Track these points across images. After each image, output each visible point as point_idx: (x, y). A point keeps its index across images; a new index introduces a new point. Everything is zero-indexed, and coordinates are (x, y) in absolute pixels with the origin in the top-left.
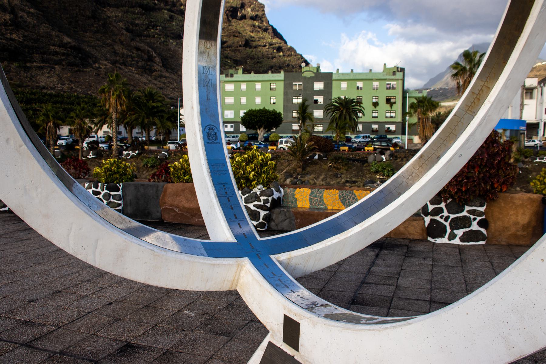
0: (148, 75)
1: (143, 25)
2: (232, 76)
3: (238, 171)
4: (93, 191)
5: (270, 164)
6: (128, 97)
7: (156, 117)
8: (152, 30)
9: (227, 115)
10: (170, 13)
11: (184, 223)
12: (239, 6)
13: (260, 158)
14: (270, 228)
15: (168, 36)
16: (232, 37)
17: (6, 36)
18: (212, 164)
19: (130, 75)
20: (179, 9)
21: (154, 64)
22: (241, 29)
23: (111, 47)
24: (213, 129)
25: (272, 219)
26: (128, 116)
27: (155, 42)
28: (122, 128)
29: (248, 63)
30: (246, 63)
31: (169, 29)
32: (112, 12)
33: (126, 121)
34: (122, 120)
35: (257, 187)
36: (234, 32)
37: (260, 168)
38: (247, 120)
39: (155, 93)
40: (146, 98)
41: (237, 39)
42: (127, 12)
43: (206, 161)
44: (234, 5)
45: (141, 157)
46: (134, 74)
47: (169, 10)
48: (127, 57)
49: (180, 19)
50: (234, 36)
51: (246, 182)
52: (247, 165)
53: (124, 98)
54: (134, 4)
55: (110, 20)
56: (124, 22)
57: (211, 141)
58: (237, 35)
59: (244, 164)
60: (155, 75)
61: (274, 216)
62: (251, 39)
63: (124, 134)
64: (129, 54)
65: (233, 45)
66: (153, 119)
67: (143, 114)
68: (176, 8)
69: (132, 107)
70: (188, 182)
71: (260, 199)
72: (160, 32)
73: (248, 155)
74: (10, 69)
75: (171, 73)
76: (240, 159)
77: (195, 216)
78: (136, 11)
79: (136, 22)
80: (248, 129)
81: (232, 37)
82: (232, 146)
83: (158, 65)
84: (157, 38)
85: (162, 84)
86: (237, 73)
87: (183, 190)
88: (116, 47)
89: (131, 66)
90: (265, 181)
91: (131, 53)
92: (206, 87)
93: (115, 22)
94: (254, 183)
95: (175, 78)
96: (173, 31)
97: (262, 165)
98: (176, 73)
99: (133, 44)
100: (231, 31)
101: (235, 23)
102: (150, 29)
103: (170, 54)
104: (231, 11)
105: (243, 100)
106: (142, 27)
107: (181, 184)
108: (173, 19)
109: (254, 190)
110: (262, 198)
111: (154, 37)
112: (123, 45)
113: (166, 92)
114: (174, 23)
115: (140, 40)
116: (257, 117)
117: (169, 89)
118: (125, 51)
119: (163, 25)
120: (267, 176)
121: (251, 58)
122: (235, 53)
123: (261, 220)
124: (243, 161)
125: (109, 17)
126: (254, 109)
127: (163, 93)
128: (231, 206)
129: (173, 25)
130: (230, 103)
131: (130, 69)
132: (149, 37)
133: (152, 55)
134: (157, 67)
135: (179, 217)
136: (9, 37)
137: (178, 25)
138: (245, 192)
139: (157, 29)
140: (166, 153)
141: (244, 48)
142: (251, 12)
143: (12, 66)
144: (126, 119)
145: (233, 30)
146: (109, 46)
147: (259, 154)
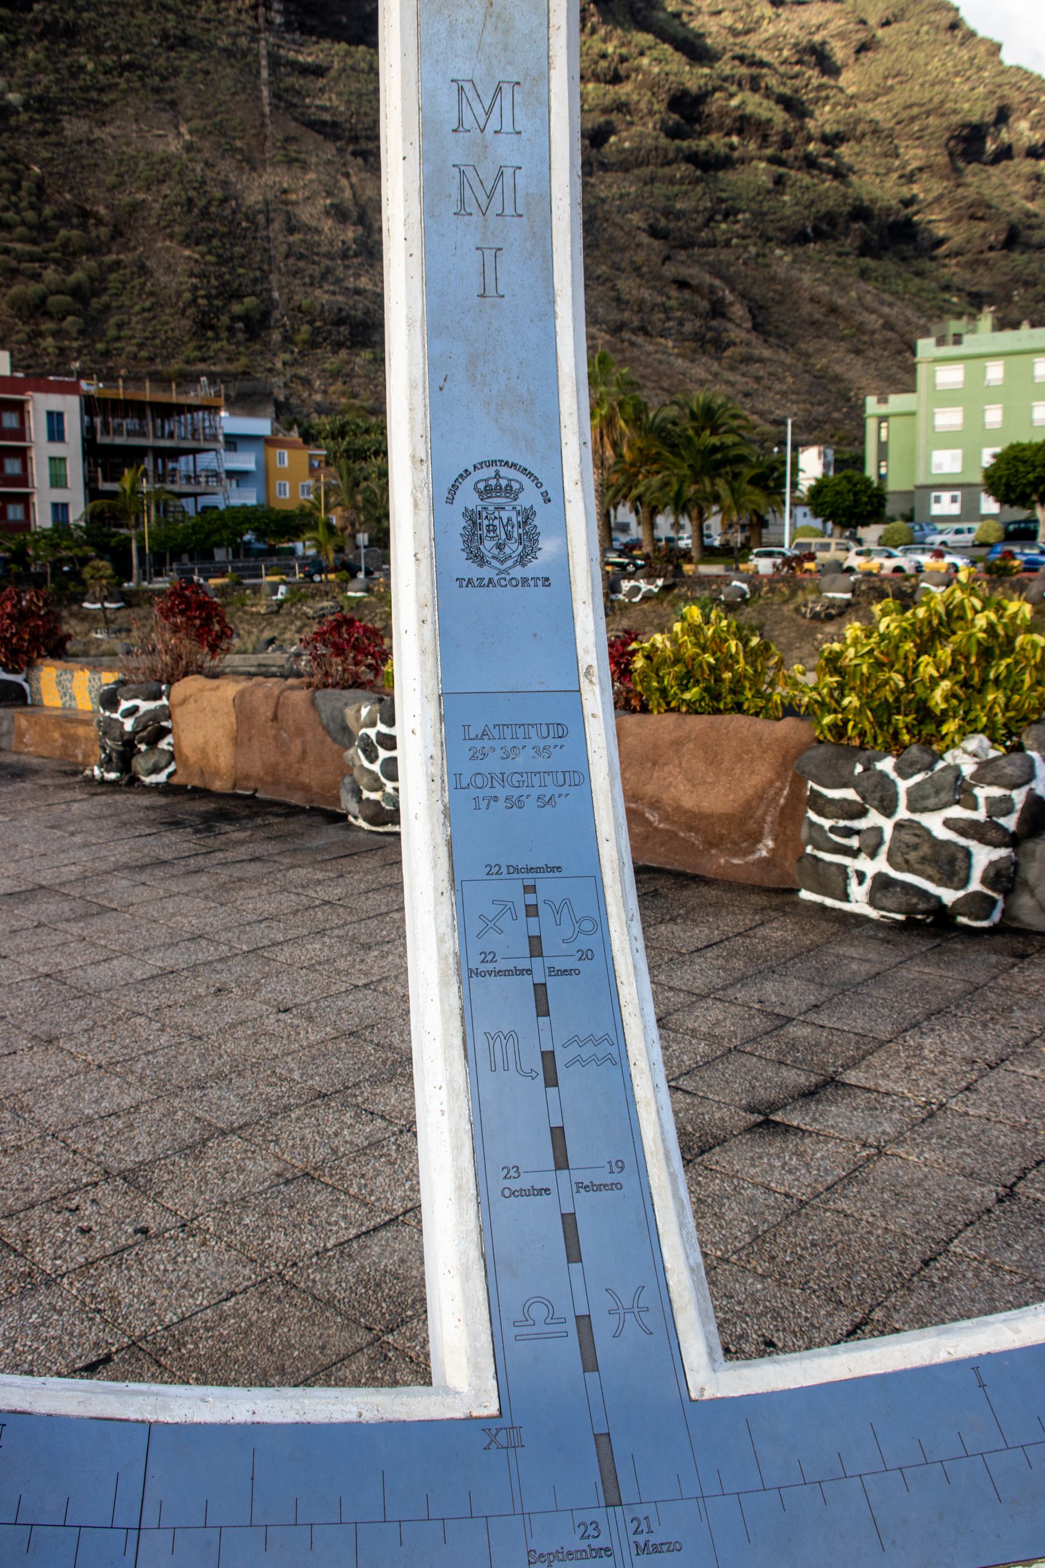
0: (712, 358)
1: (697, 212)
2: (958, 340)
3: (882, 676)
4: (379, 734)
5: (1023, 649)
6: (636, 420)
7: (720, 476)
8: (723, 226)
9: (940, 466)
10: (774, 168)
11: (677, 866)
12: (990, 119)
13: (981, 621)
14: (1014, 919)
15: (769, 239)
16: (965, 221)
17: (347, 284)
18: (476, 730)
19: (660, 362)
20: (801, 154)
21: (730, 326)
22: (997, 193)
23: (609, 285)
24: (508, 491)
25: (1025, 883)
26: (640, 477)
27: (733, 258)
28: (624, 514)
29: (1016, 299)
30: (1009, 299)
31: (772, 217)
32: (610, 186)
33: (635, 493)
34: (625, 490)
35: (964, 744)
36: (971, 207)
37: (977, 664)
38: (1000, 477)
39: (720, 407)
40: (695, 424)
41: (983, 226)
42: (653, 180)
43: (432, 711)
44: (975, 118)
45: (670, 597)
46: (672, 359)
47: (773, 160)
48: (652, 310)
49: (804, 183)
50: (972, 217)
51: (921, 722)
52: (921, 650)
53: (622, 423)
54: (671, 155)
55: (606, 207)
56: (643, 210)
57: (486, 572)
58: (980, 214)
59: (909, 646)
60: (731, 358)
61: (1032, 872)
62: (1029, 222)
63: (637, 532)
64: (659, 299)
65: (969, 246)
66: (713, 485)
67: (686, 471)
68: (792, 151)
69: (654, 451)
70: (697, 713)
71: (975, 798)
72: (745, 227)
73: (929, 610)
74: (353, 370)
75: (779, 346)
76: (893, 626)
77: (716, 846)
78: (678, 175)
79: (678, 206)
80: (1006, 507)
81: (965, 221)
82: (948, 559)
83: (739, 326)
84: (737, 246)
85: (750, 381)
86: (973, 331)
87: (677, 744)
88: (621, 284)
89: (662, 336)
90: (1000, 719)
91: (664, 299)
92: (476, 218)
93: (619, 211)
94: (950, 727)
95: (789, 360)
96: (784, 223)
97: (986, 654)
98: (792, 345)
99: (670, 270)
100: (963, 204)
101: (975, 175)
102: (716, 221)
103: (775, 291)
104: (965, 139)
105: (994, 416)
106: (695, 220)
107: (672, 717)
108: (784, 185)
109: (949, 757)
110: (982, 793)
111: (727, 244)
112: (641, 276)
113: (763, 403)
114: (786, 198)
115: (690, 257)
116: (1034, 467)
117: (771, 394)
118: (646, 294)
119: (754, 206)
120: (1009, 699)
121: (1027, 284)
122: (974, 271)
123: (975, 885)
124: (905, 635)
125: (603, 201)
126: (1025, 440)
127: (753, 407)
128: (548, 1057)
129: (785, 203)
130: (950, 426)
131: (660, 344)
132: (715, 246)
133: (723, 298)
134: (735, 333)
135: (663, 844)
136: (351, 286)
137: (797, 204)
138: (912, 764)
139: (736, 222)
140: (745, 586)
141: (1004, 252)
142: (1031, 134)
143: (358, 360)
144: (636, 486)
145: (969, 200)
146: (603, 284)
147: (978, 604)
